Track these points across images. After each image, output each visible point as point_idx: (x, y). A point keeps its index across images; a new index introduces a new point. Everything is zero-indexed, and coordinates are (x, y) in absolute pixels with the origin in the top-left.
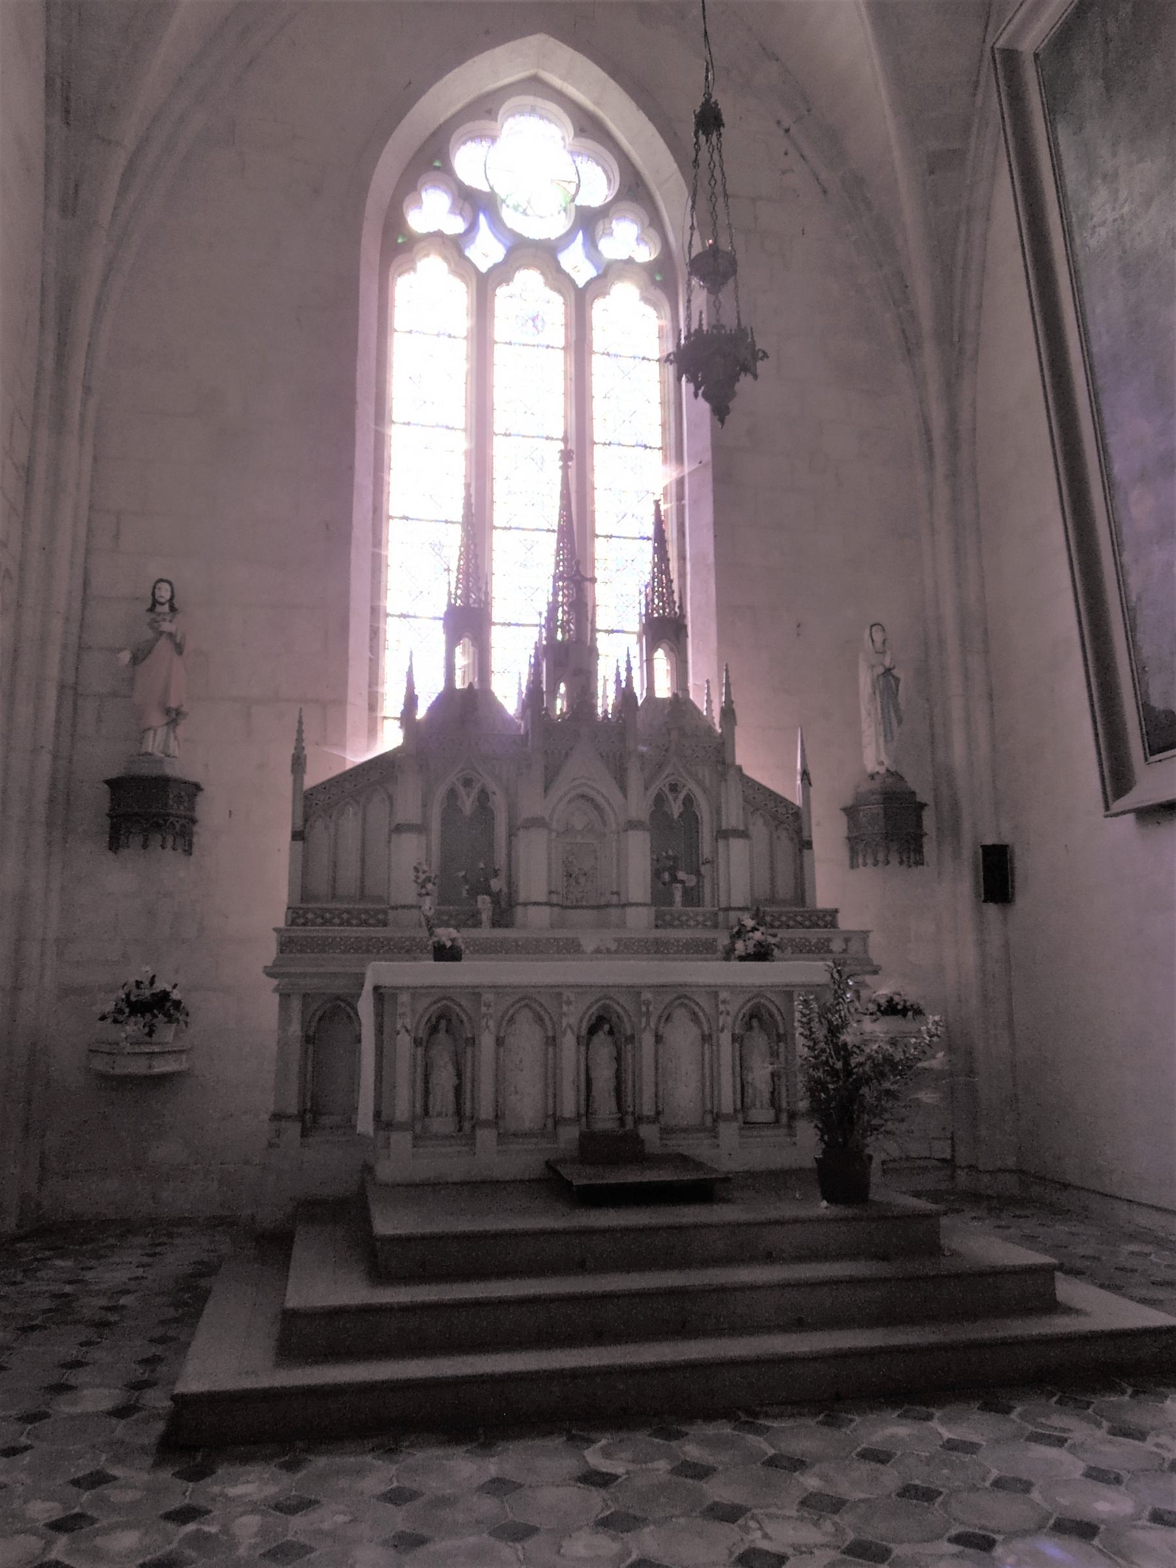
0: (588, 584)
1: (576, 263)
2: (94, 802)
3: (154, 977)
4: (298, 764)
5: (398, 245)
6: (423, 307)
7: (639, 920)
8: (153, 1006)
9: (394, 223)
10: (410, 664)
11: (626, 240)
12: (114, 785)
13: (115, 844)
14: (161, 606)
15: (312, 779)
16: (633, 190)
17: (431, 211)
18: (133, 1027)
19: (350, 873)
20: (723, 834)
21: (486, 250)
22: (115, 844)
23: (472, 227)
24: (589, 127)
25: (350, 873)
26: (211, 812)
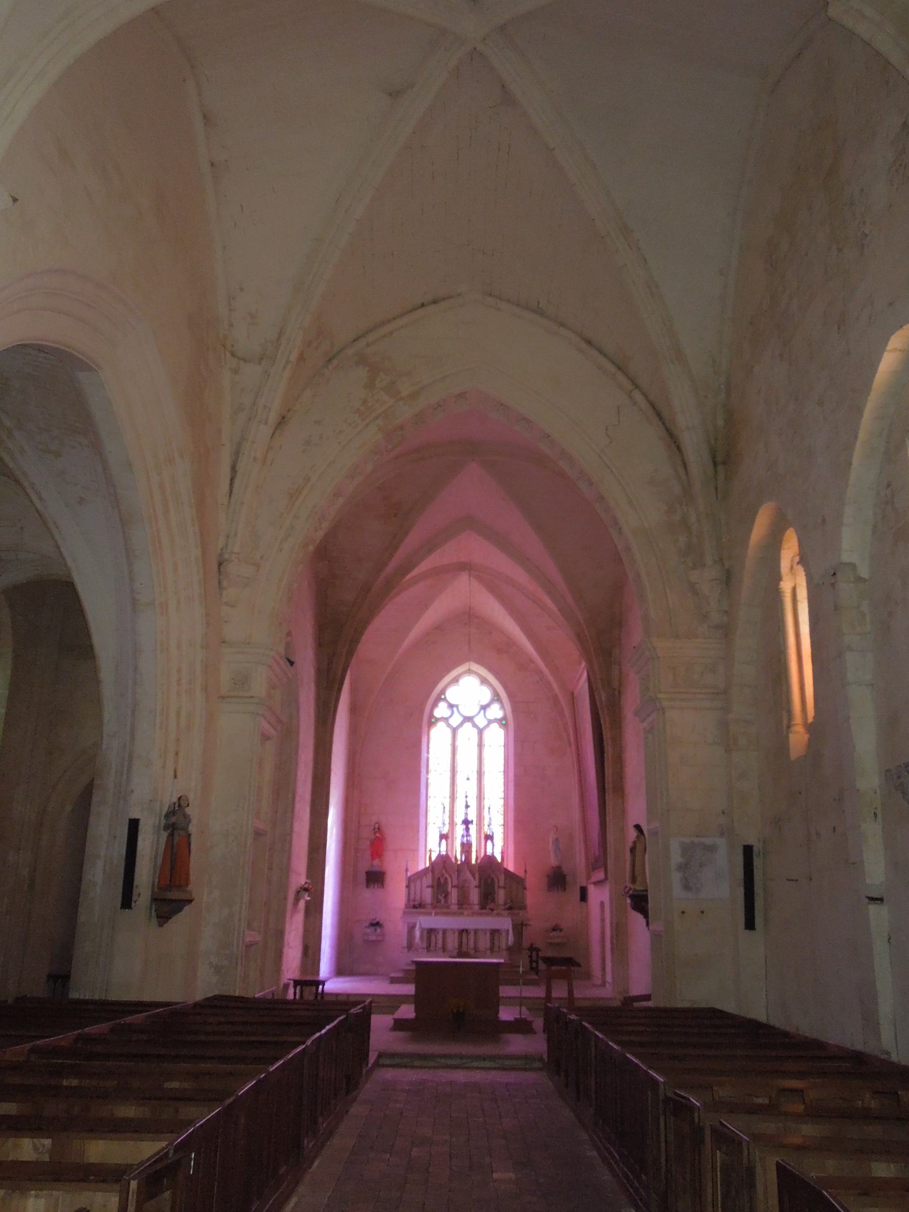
0: (326, 998)
1: (481, 721)
2: (363, 877)
3: (868, 898)
4: (407, 870)
5: (432, 722)
6: (437, 741)
7: (477, 908)
8: (376, 924)
9: (431, 715)
10: (433, 847)
11: (496, 711)
12: (366, 873)
13: (367, 886)
14: (378, 829)
15: (409, 874)
16: (496, 698)
17: (441, 711)
18: (372, 929)
19: (418, 898)
20: (499, 887)
21: (455, 721)
22: (367, 886)
23: (453, 713)
24: (484, 681)
25: (418, 898)
26: (388, 879)
